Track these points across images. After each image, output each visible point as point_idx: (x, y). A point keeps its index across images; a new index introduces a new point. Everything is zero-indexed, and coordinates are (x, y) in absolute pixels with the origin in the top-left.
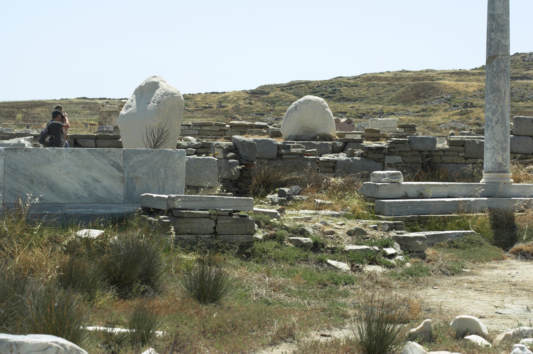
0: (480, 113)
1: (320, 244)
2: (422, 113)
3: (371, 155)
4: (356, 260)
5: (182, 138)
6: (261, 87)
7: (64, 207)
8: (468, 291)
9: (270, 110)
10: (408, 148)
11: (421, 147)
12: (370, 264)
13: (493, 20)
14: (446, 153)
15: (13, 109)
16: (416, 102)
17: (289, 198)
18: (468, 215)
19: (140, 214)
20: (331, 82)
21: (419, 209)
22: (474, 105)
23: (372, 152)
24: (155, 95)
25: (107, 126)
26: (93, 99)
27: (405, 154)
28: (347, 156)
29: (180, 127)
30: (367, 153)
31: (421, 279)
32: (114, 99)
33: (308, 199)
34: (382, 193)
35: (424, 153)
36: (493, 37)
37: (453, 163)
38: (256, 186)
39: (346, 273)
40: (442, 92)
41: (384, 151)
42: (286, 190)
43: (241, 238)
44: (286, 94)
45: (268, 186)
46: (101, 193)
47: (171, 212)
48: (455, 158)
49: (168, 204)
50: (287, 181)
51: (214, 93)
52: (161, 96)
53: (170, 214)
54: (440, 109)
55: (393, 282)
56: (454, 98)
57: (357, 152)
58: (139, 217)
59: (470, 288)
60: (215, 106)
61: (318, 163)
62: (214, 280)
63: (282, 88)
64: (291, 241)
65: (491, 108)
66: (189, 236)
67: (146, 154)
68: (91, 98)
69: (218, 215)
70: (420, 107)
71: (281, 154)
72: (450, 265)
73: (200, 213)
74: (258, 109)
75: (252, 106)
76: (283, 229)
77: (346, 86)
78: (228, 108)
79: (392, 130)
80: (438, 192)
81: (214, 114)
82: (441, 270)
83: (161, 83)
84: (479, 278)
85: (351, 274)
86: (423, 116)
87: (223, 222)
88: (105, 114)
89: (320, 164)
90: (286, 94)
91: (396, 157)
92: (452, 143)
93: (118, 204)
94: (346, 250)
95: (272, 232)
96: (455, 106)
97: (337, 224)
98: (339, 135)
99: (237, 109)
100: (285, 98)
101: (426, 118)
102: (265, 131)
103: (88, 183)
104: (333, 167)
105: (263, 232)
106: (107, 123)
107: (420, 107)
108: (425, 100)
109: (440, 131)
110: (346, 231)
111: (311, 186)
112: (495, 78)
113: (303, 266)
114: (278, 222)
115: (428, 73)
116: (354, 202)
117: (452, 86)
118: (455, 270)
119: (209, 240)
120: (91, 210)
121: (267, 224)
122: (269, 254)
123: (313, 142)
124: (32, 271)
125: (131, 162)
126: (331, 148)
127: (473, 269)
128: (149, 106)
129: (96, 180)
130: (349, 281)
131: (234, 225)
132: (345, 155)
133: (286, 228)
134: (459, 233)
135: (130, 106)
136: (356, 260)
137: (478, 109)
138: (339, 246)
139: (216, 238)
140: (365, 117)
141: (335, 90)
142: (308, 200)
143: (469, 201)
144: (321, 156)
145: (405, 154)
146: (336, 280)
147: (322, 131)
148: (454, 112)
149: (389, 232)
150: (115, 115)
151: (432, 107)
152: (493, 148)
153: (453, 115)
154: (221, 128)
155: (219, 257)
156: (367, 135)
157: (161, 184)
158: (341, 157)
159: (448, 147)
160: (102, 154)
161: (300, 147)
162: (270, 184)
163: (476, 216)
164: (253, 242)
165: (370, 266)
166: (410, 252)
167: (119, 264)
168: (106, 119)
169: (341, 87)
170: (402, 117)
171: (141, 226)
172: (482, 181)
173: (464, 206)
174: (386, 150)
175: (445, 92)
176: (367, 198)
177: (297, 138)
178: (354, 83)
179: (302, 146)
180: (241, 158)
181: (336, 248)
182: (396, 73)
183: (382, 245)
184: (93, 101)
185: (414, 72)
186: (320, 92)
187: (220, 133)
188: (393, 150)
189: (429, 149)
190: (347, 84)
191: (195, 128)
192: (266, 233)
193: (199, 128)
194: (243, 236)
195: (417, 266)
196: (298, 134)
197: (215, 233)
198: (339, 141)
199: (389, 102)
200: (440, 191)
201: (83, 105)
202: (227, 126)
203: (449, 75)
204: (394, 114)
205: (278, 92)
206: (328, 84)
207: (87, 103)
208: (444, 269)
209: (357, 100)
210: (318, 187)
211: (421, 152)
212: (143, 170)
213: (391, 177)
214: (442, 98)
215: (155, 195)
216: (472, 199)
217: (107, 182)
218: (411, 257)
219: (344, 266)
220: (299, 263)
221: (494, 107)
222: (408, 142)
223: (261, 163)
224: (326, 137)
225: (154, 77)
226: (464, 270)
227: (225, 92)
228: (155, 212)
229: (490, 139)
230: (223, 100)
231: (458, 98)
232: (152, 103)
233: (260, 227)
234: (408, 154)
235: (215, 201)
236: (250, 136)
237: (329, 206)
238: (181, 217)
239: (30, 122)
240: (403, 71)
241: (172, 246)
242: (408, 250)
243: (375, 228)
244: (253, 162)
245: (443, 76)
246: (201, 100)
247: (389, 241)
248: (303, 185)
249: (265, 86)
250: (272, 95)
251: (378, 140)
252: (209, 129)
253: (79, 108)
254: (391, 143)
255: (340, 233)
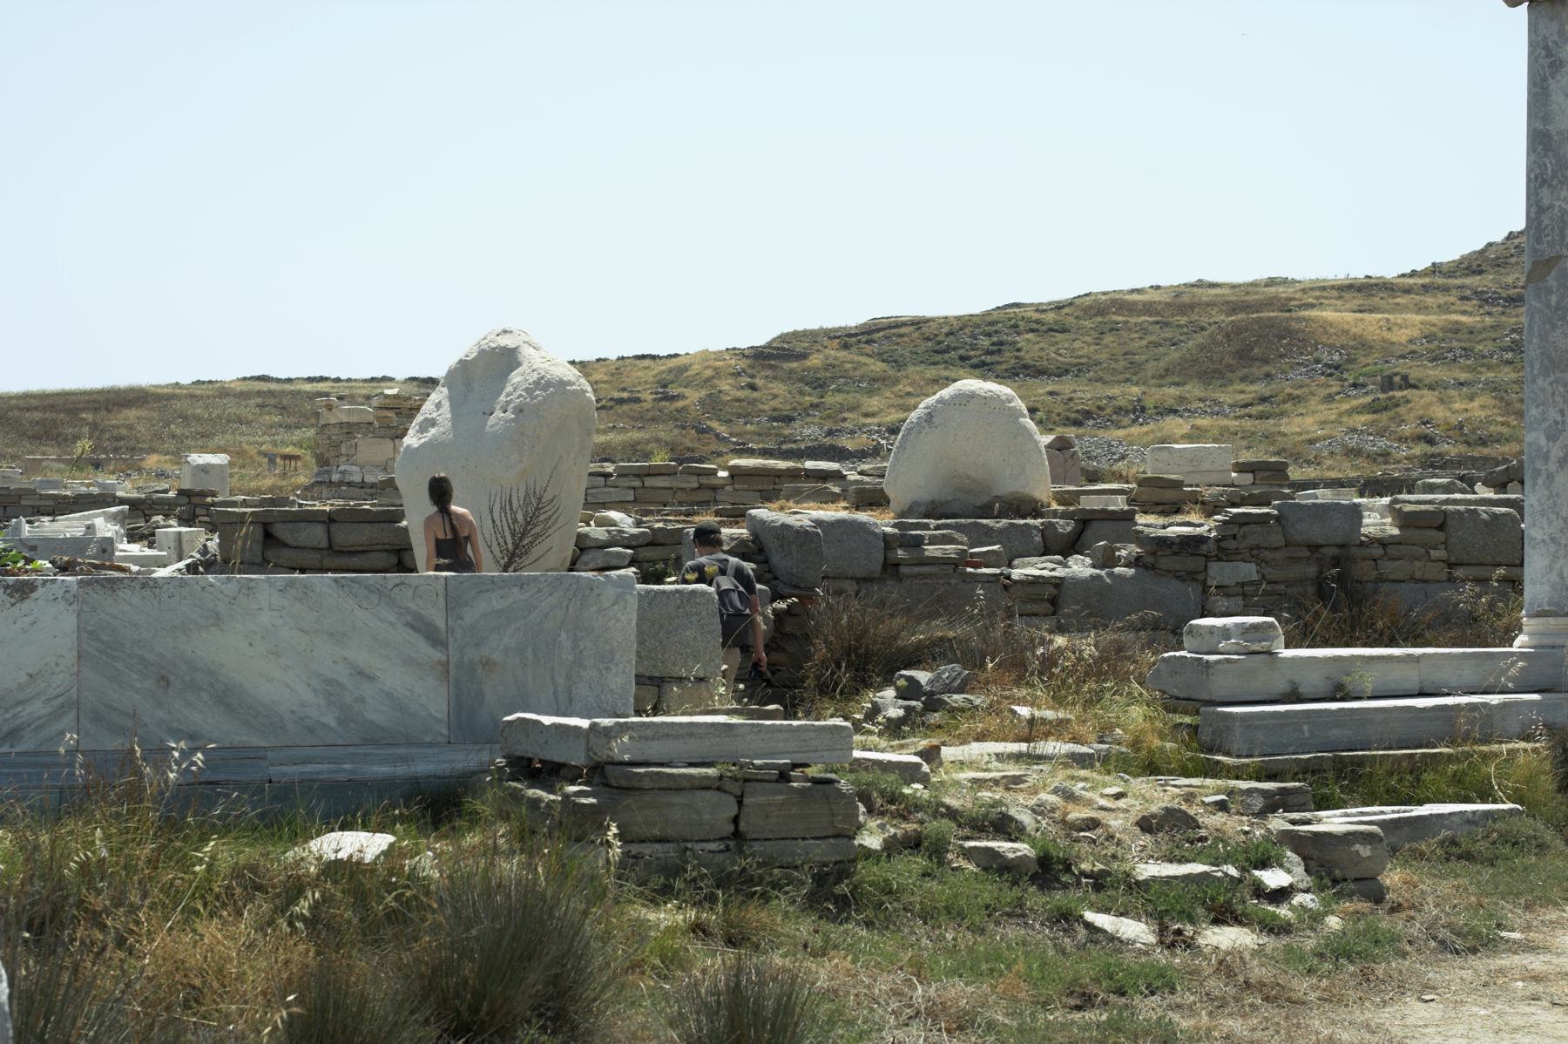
0: (1430, 404)
1: (1059, 861)
2: (1261, 408)
3: (1166, 562)
4: (1170, 908)
5: (592, 517)
6: (783, 338)
7: (264, 758)
8: (1532, 1009)
9: (812, 406)
10: (1277, 539)
11: (1316, 533)
12: (1217, 922)
13: (1546, 150)
14: (1392, 550)
15: (53, 415)
16: (1240, 374)
17: (933, 704)
18: (1485, 748)
19: (500, 780)
20: (988, 319)
21: (1335, 733)
22: (1412, 382)
23: (1168, 552)
24: (509, 388)
25: (342, 468)
26: (289, 380)
27: (1267, 555)
28: (1094, 566)
29: (585, 482)
30: (1154, 554)
31: (1380, 970)
32: (349, 380)
33: (991, 706)
34: (1220, 685)
35: (1324, 550)
36: (1546, 202)
37: (1413, 579)
38: (824, 663)
39: (1146, 953)
40: (1317, 343)
41: (1204, 547)
42: (923, 677)
43: (818, 851)
44: (857, 358)
45: (867, 664)
46: (377, 714)
47: (599, 772)
48: (1418, 564)
49: (589, 749)
50: (919, 646)
51: (643, 357)
52: (526, 390)
53: (596, 780)
54: (1312, 394)
55: (1295, 983)
56: (1350, 361)
57: (1124, 553)
58: (500, 786)
59: (1535, 998)
60: (648, 396)
61: (1006, 587)
62: (776, 1013)
63: (847, 338)
64: (968, 854)
65: (1545, 419)
66: (657, 846)
67: (516, 590)
68: (283, 376)
69: (746, 781)
70: (1259, 388)
71: (893, 563)
72: (1461, 920)
73: (691, 776)
74: (775, 403)
75: (756, 395)
76: (942, 815)
77: (1032, 331)
78: (685, 403)
79: (1215, 478)
80: (1393, 679)
81: (642, 420)
82: (1435, 938)
83: (526, 351)
84: (1556, 961)
85: (1161, 957)
86: (1262, 416)
87: (762, 800)
88: (336, 431)
89: (1012, 590)
90: (857, 358)
91: (1242, 564)
92: (1407, 521)
93: (430, 745)
94: (1141, 878)
95: (911, 827)
96: (1355, 385)
97: (1102, 796)
98: (1062, 498)
99: (713, 404)
100: (855, 369)
101: (1272, 421)
102: (837, 490)
103: (339, 684)
104: (1051, 600)
105: (882, 827)
106: (343, 459)
107: (1259, 388)
108: (1266, 368)
109: (1317, 461)
110: (1133, 818)
111: (999, 665)
112: (1554, 327)
113: (1013, 932)
114: (926, 794)
115: (1272, 289)
116: (1135, 716)
117: (1346, 327)
118: (1478, 936)
119: (720, 857)
120: (346, 766)
121: (891, 802)
122: (906, 898)
123: (984, 521)
124: (194, 998)
125: (470, 616)
126: (1038, 539)
127: (1528, 928)
128: (492, 420)
129: (362, 674)
130: (1160, 983)
131: (794, 810)
132: (1088, 561)
133: (952, 814)
134: (1474, 812)
135: (433, 423)
136: (1170, 908)
137: (1425, 392)
138: (1115, 866)
139: (740, 851)
140: (1091, 422)
141: (1001, 343)
142: (991, 709)
143: (1485, 705)
144: (1010, 566)
145: (1267, 555)
146: (1122, 979)
147: (1009, 486)
148: (1355, 403)
149: (1266, 818)
150: (365, 435)
151: (1289, 390)
152: (1553, 539)
153: (1350, 412)
154: (704, 480)
155: (755, 914)
156: (1145, 498)
157: (561, 681)
158: (1075, 568)
159: (1396, 532)
160: (380, 593)
161: (952, 541)
162: (867, 657)
163: (1509, 751)
164: (854, 861)
165: (1216, 929)
166: (1335, 882)
167: (468, 969)
168: (338, 446)
169: (1019, 334)
170: (1199, 422)
171: (506, 817)
172: (1521, 642)
173: (1472, 722)
174: (1212, 546)
175: (1325, 345)
176: (1173, 704)
177: (935, 510)
178: (1056, 322)
179: (957, 535)
180: (776, 578)
181: (1109, 874)
182: (1178, 291)
183: (1248, 859)
184: (288, 387)
185: (1233, 286)
186: (955, 349)
187: (703, 496)
188: (1231, 544)
189: (1339, 540)
190: (1035, 326)
191: (624, 482)
192: (892, 830)
193: (637, 483)
194: (823, 844)
195: (1361, 926)
196: (936, 497)
197: (737, 834)
198: (1064, 515)
199: (1162, 377)
200: (1396, 676)
201: (259, 400)
202: (723, 474)
203: (1335, 293)
204: (1175, 412)
205: (834, 353)
206: (978, 326)
207: (271, 393)
208: (1443, 934)
209: (1067, 371)
210: (1018, 668)
211: (1314, 548)
212: (506, 640)
213: (1248, 636)
214: (1318, 361)
215: (547, 720)
216: (1495, 699)
217: (395, 679)
218: (1339, 895)
219: (1136, 930)
220: (997, 923)
221: (1553, 414)
222: (1277, 518)
223: (838, 593)
224: (1026, 507)
225: (505, 332)
226: (1503, 934)
227: (676, 355)
228: (550, 773)
229: (1543, 513)
230: (671, 377)
231: (1363, 360)
232: (498, 414)
233: (870, 811)
234: (1278, 555)
235: (735, 736)
236: (791, 504)
237: (1056, 729)
238: (631, 788)
239: (106, 452)
240: (1200, 284)
241: (609, 881)
242: (1329, 874)
243: (1222, 806)
244: (812, 589)
245: (1317, 298)
246: (606, 378)
247: (1269, 846)
248: (973, 660)
249: (795, 334)
250: (815, 360)
251: (1178, 511)
252: (667, 484)
253: (248, 410)
254: (1225, 522)
255: (1115, 823)
